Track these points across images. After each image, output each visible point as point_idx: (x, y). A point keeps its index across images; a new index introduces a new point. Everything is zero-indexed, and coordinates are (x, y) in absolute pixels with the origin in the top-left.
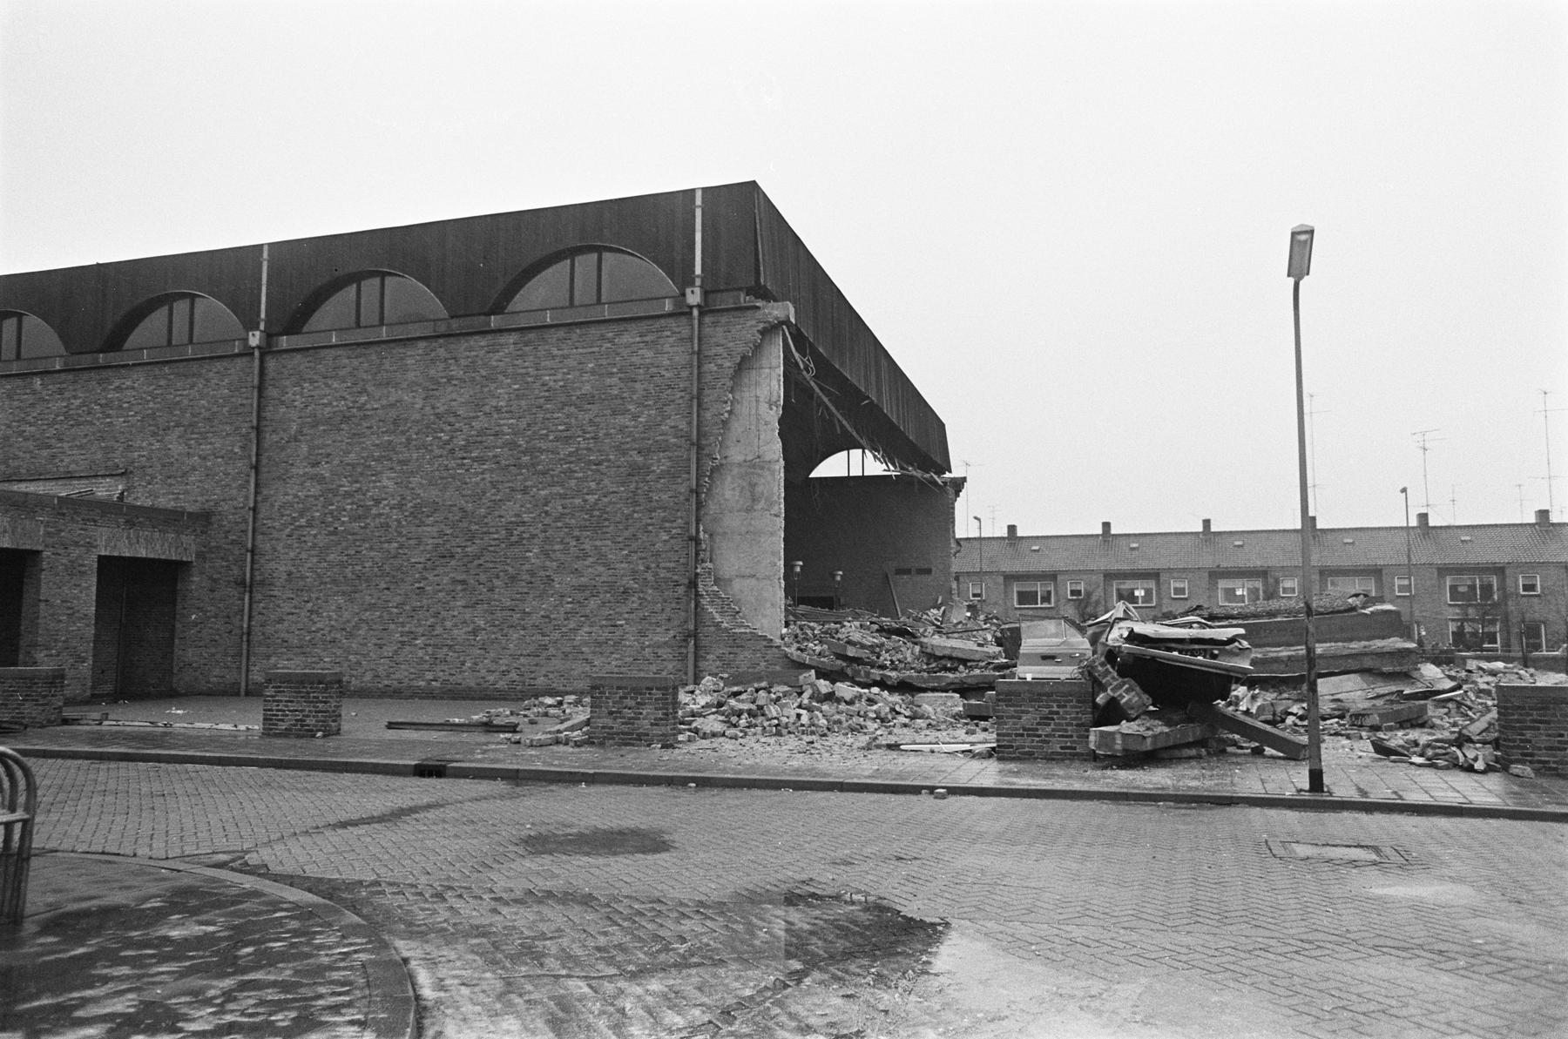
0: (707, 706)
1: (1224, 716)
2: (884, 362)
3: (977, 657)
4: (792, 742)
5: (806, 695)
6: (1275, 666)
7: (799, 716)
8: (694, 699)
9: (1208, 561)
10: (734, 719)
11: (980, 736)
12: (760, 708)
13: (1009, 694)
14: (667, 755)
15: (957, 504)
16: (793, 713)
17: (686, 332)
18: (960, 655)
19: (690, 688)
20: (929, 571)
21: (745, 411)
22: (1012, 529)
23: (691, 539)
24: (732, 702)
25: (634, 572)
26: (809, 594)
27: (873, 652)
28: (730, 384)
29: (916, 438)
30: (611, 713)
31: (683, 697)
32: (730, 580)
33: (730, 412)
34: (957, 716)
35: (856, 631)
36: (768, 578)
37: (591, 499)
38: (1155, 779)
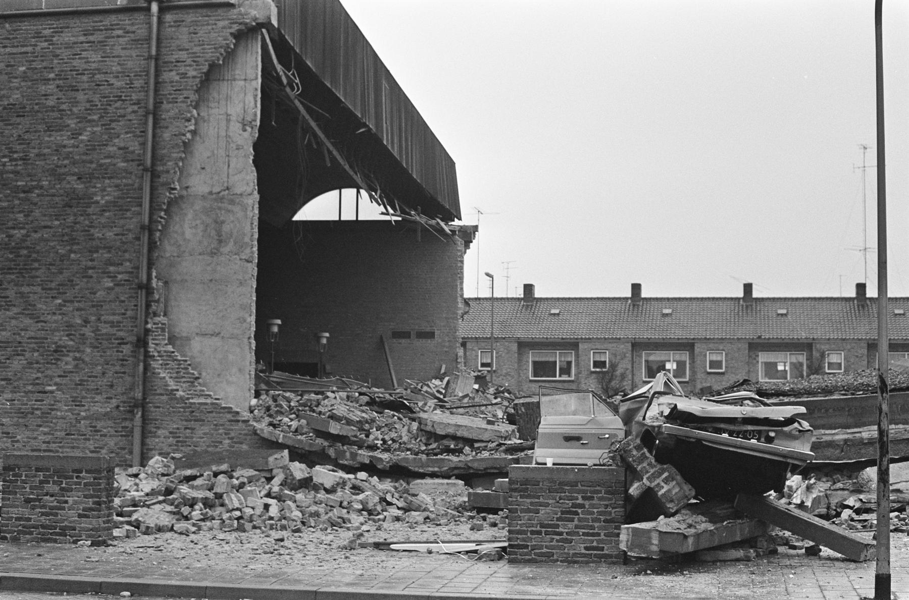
0: (153, 493)
1: (776, 509)
2: (385, 84)
3: (485, 437)
4: (256, 539)
5: (276, 481)
6: (829, 452)
7: (267, 507)
8: (132, 485)
9: (747, 331)
10: (185, 510)
11: (487, 533)
12: (219, 496)
13: (526, 482)
14: (97, 554)
15: (466, 257)
16: (259, 503)
17: (142, 32)
18: (466, 434)
19: (134, 470)
20: (431, 335)
21: (212, 132)
22: (529, 288)
23: (140, 287)
24: (184, 489)
25: (69, 326)
26: (284, 356)
27: (361, 429)
28: (194, 97)
29: (421, 186)
30: (28, 501)
31: (122, 480)
32: (188, 339)
33: (194, 133)
34: (461, 509)
35: (339, 403)
36: (233, 337)
37: (18, 234)
38: (697, 588)
